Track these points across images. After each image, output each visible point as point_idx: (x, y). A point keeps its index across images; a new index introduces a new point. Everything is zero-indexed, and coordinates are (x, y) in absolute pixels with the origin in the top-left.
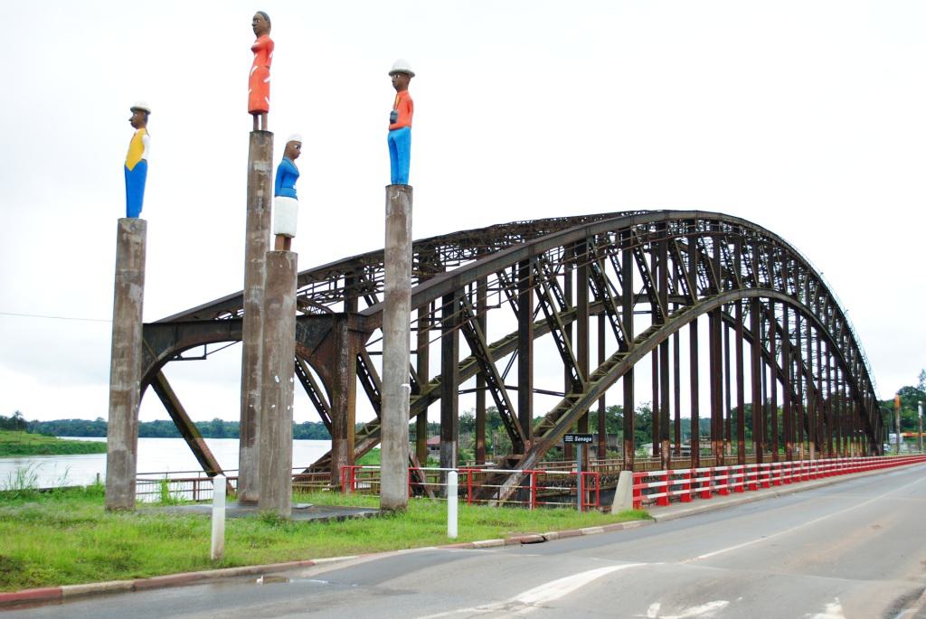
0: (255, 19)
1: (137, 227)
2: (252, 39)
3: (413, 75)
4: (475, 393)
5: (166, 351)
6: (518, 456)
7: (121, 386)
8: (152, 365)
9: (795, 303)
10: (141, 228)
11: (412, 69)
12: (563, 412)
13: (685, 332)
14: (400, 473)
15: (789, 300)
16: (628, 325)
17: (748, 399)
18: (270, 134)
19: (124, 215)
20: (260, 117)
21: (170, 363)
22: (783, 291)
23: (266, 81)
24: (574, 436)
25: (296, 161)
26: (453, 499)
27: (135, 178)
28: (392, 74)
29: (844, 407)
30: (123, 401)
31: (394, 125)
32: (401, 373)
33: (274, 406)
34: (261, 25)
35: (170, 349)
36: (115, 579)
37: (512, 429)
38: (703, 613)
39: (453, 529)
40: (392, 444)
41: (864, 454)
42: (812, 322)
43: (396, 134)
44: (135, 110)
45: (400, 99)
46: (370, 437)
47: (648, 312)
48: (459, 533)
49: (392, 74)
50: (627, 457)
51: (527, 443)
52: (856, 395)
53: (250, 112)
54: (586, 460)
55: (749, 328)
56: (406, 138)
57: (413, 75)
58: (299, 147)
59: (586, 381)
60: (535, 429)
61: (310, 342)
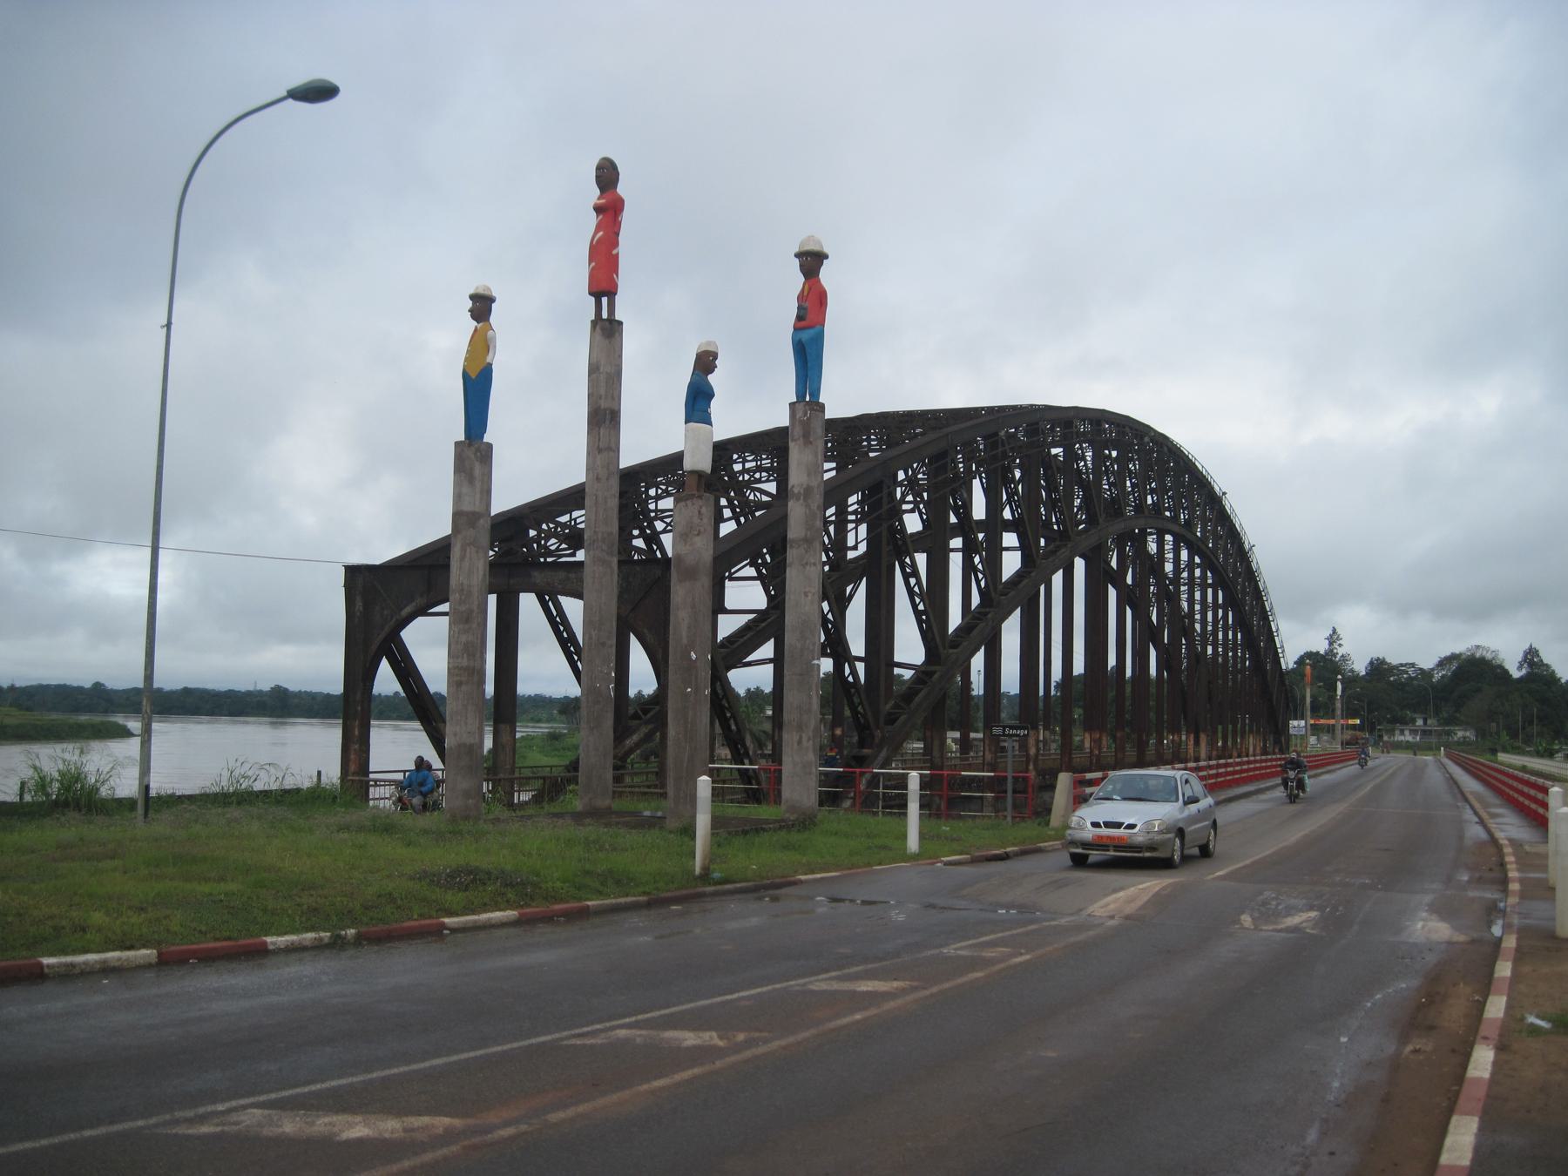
0: (598, 168)
1: (483, 453)
2: (593, 194)
3: (826, 257)
4: (772, 665)
5: (414, 604)
6: (866, 751)
7: (465, 660)
8: (392, 623)
9: (1189, 536)
10: (486, 454)
11: (826, 250)
12: (917, 692)
13: (1058, 579)
14: (810, 774)
15: (1183, 531)
16: (994, 564)
17: (1079, 667)
18: (620, 323)
19: (462, 438)
20: (605, 300)
21: (420, 619)
22: (1175, 518)
23: (614, 252)
24: (1004, 727)
25: (711, 378)
26: (913, 808)
27: (477, 387)
28: (797, 255)
29: (1235, 680)
30: (359, 670)
31: (803, 324)
32: (811, 648)
33: (689, 690)
34: (607, 175)
35: (419, 601)
36: (627, 896)
37: (722, 707)
38: (1302, 923)
39: (913, 843)
40: (801, 737)
41: (1265, 752)
42: (1208, 564)
43: (805, 335)
44: (473, 297)
45: (810, 289)
46: (647, 722)
47: (1007, 549)
48: (920, 847)
49: (797, 255)
50: (987, 753)
51: (878, 733)
52: (1258, 665)
53: (591, 294)
54: (514, 762)
55: (834, 507)
56: (819, 340)
57: (826, 257)
58: (715, 357)
59: (945, 649)
60: (631, 711)
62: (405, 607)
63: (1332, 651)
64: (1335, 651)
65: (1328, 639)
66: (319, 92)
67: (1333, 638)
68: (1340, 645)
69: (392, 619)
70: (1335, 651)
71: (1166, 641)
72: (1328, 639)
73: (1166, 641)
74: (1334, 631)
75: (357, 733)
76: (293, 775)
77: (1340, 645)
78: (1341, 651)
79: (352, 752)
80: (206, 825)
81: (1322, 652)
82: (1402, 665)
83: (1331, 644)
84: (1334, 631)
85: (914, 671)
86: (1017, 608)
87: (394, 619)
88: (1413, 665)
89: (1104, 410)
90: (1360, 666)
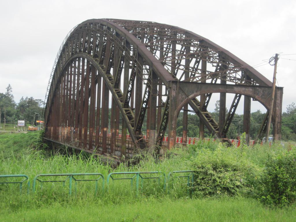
61: (263, 96)
62: (190, 95)
63: (8, 93)
64: (9, 93)
65: (7, 88)
66: (276, 58)
67: (9, 88)
68: (11, 91)
69: (185, 99)
70: (9, 93)
71: (69, 83)
72: (7, 88)
73: (69, 83)
74: (9, 86)
75: (172, 134)
76: (164, 175)
77: (11, 91)
78: (11, 93)
79: (171, 140)
80: (64, 181)
81: (4, 94)
82: (36, 100)
83: (8, 90)
84: (9, 86)
85: (200, 96)
86: (200, 101)
87: (186, 99)
88: (20, 100)
89: (93, 19)
90: (17, 101)
